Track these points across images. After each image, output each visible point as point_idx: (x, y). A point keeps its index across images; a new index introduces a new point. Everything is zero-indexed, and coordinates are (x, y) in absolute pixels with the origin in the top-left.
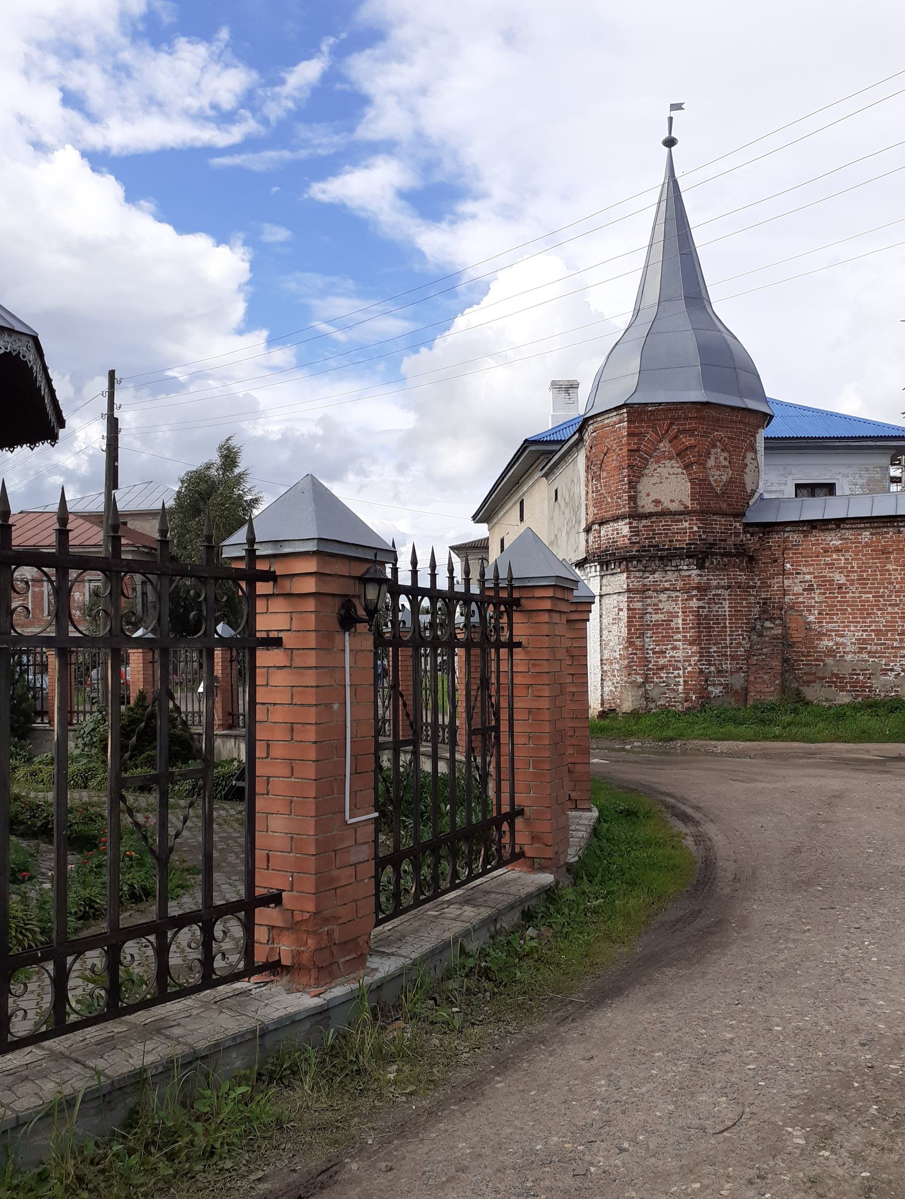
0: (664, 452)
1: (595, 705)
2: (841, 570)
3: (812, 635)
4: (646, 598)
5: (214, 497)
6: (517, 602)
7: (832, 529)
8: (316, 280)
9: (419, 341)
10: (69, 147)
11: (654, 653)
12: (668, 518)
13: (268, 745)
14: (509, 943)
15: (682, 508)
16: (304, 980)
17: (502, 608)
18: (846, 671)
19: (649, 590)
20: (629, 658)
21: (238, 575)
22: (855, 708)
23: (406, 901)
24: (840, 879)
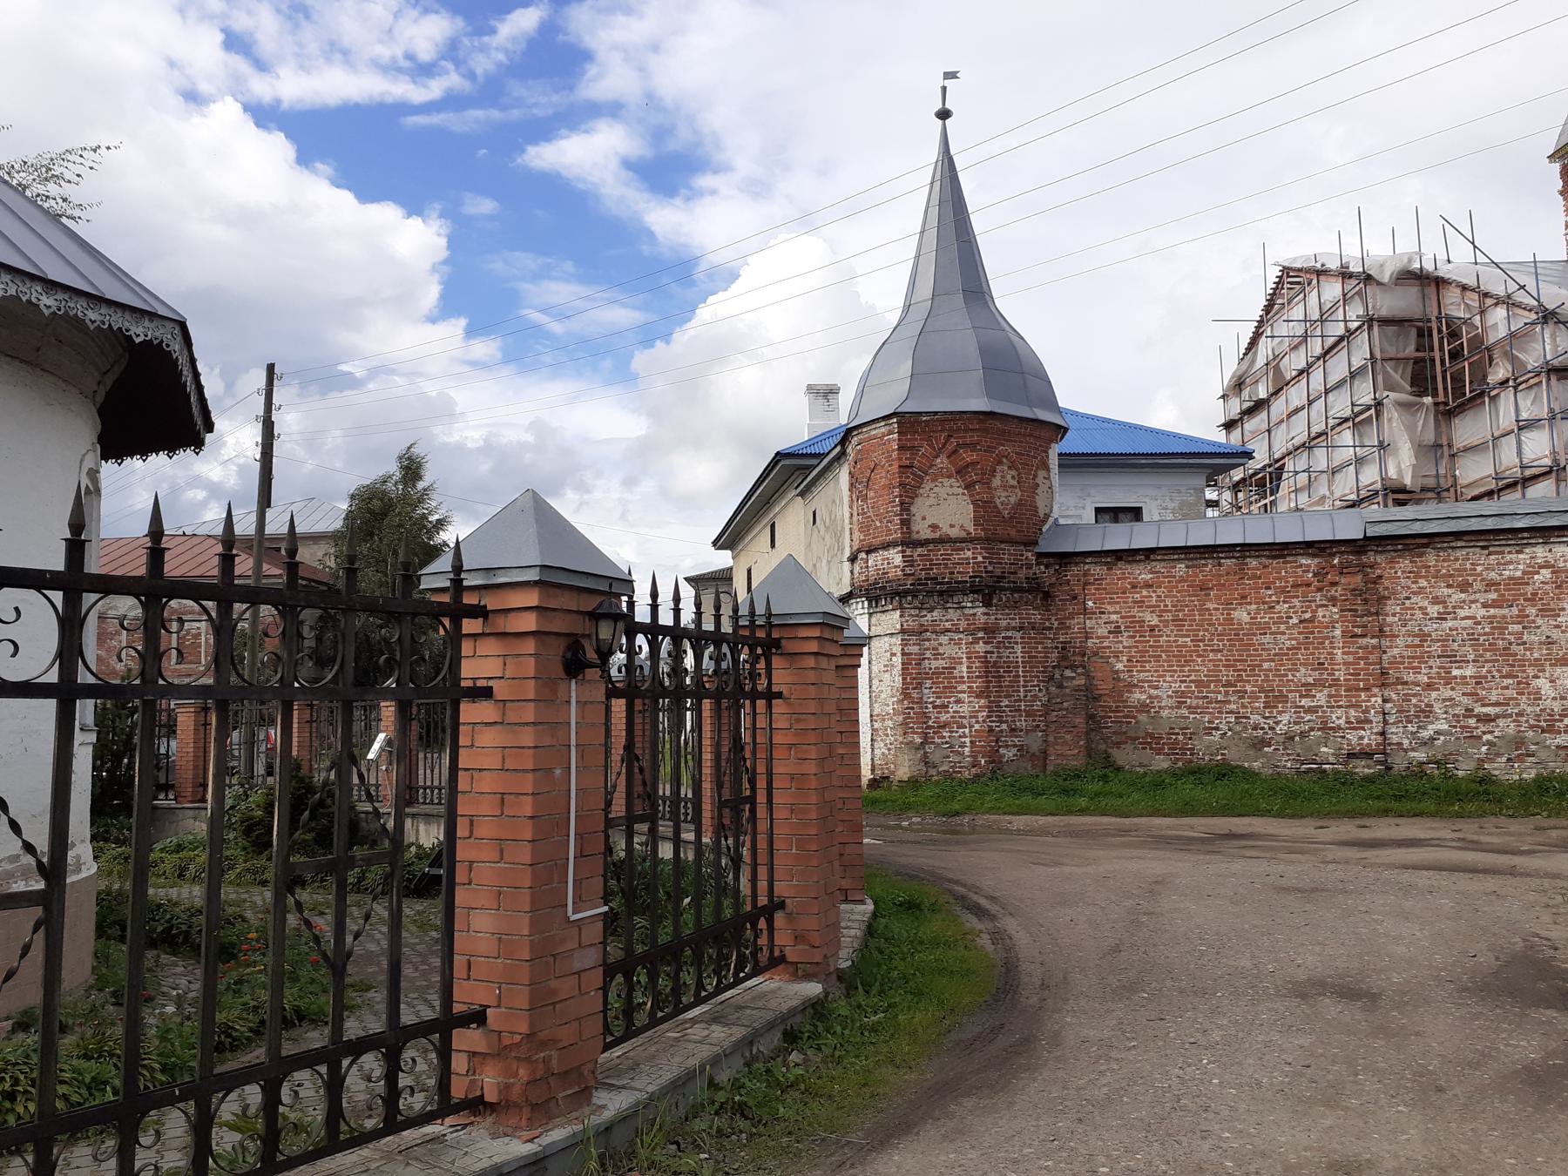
1: (866, 774)
2: (1152, 609)
5: (390, 518)
6: (777, 643)
8: (527, 261)
9: (650, 336)
10: (229, 99)
13: (472, 822)
14: (768, 1071)
15: (963, 534)
16: (513, 1121)
17: (759, 651)
21: (437, 612)
22: (1175, 774)
23: (641, 1019)
24: (1169, 984)
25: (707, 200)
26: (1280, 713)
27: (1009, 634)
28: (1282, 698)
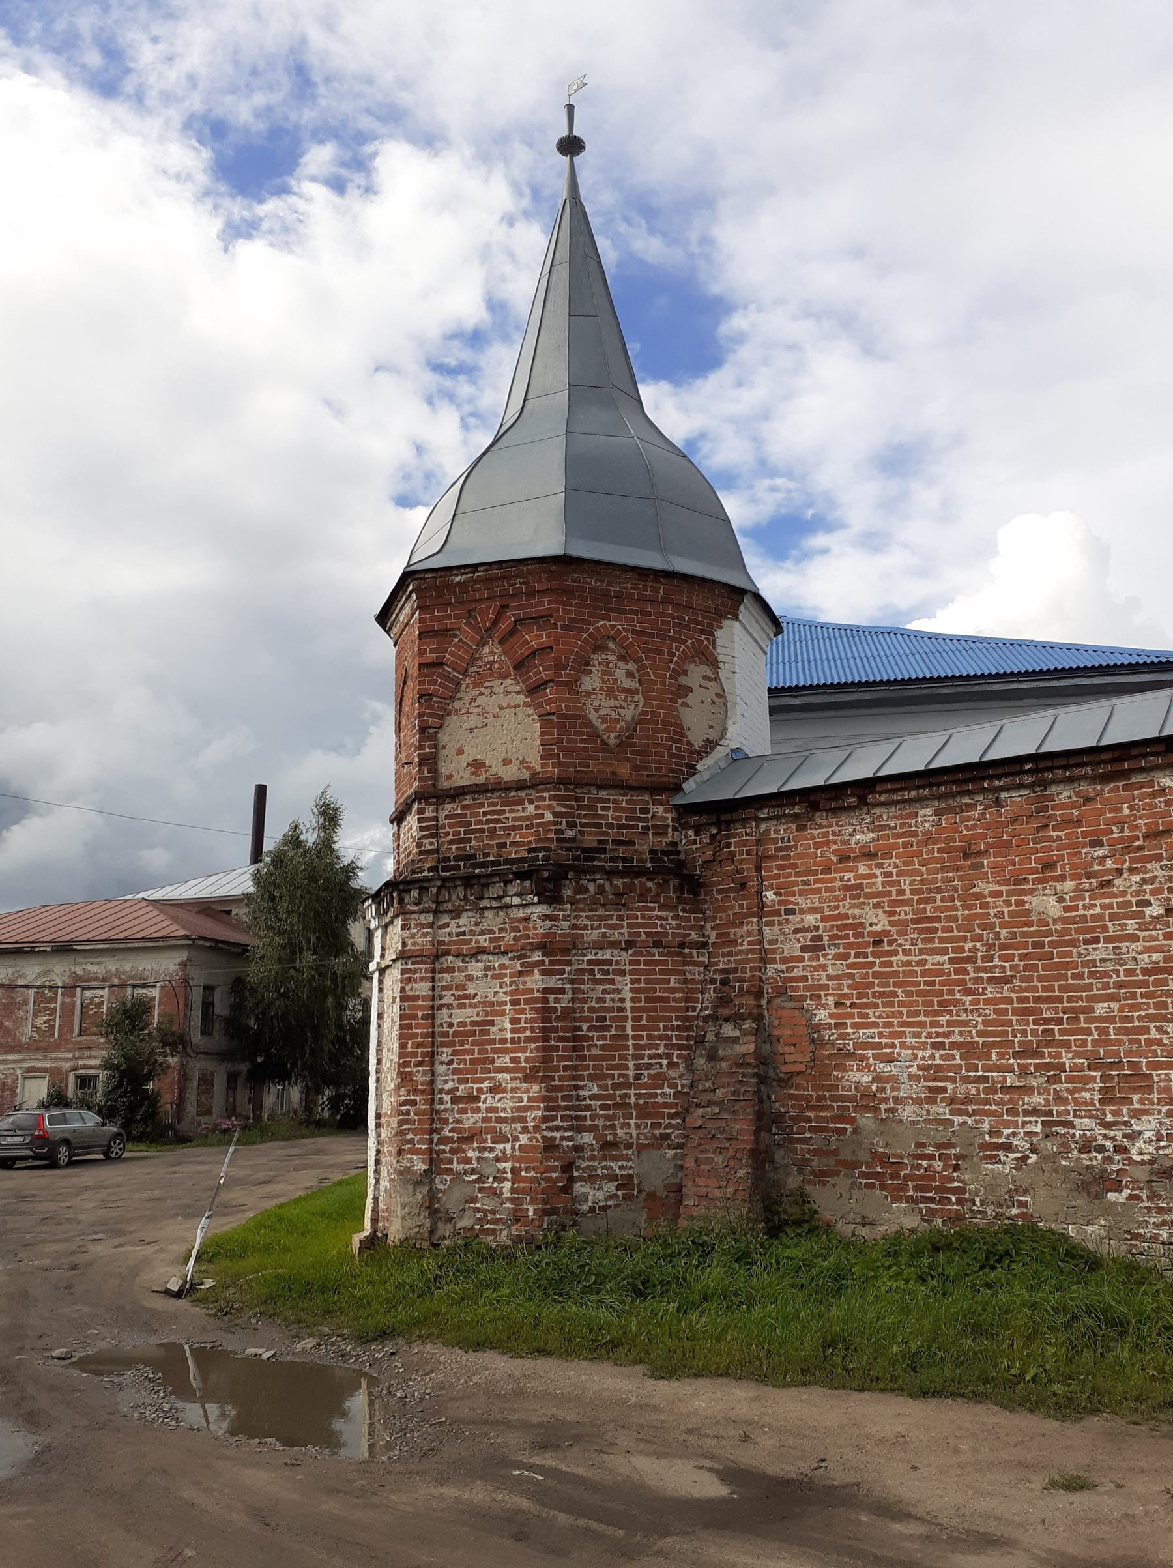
0: (491, 663)
3: (827, 1058)
4: (442, 971)
7: (851, 808)
11: (455, 1100)
12: (495, 797)
15: (526, 775)
18: (903, 1148)
19: (448, 953)
20: (400, 1113)
25: (818, 561)
26: (1136, 1114)
27: (606, 955)
28: (1140, 1081)
